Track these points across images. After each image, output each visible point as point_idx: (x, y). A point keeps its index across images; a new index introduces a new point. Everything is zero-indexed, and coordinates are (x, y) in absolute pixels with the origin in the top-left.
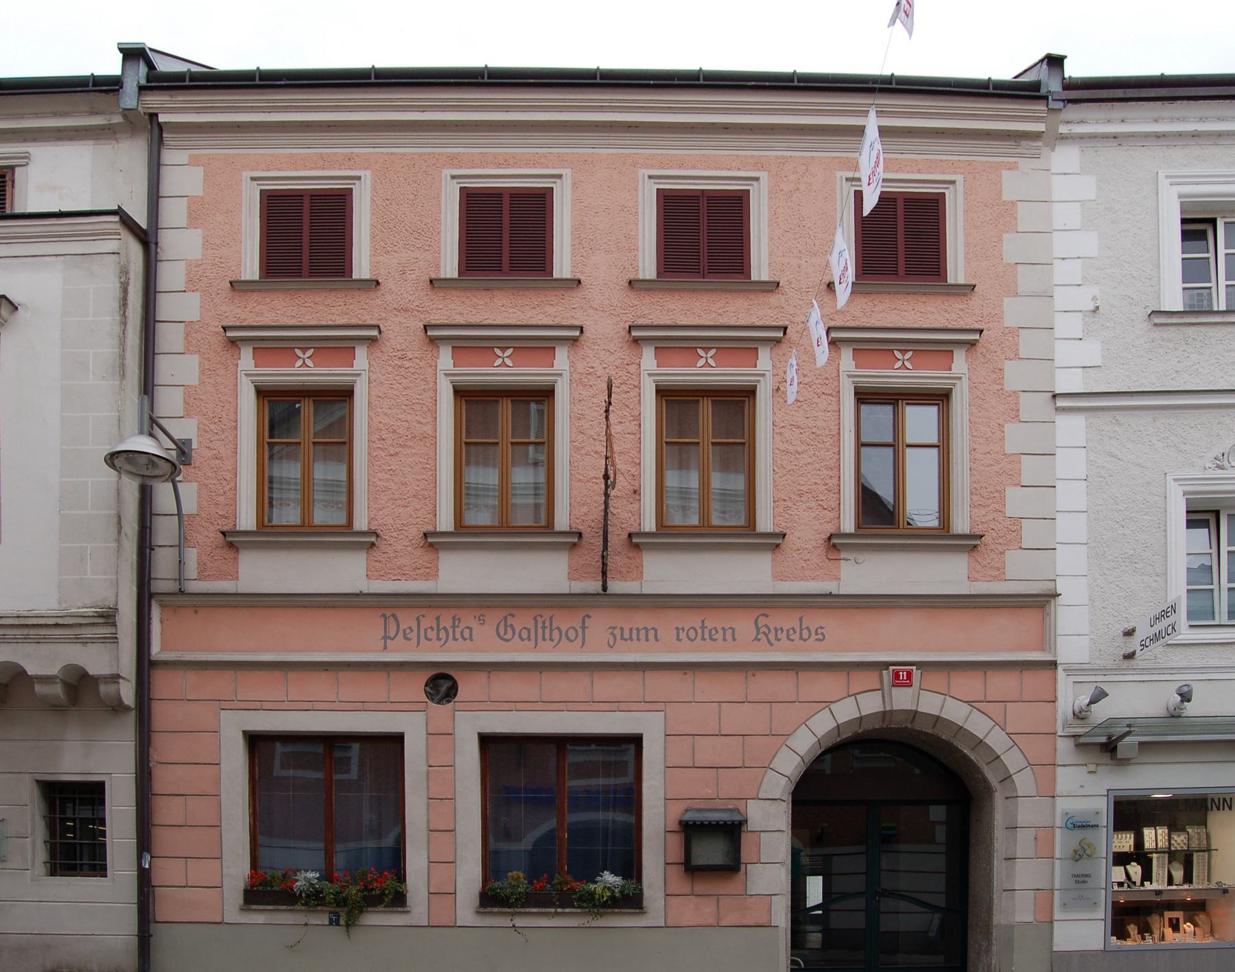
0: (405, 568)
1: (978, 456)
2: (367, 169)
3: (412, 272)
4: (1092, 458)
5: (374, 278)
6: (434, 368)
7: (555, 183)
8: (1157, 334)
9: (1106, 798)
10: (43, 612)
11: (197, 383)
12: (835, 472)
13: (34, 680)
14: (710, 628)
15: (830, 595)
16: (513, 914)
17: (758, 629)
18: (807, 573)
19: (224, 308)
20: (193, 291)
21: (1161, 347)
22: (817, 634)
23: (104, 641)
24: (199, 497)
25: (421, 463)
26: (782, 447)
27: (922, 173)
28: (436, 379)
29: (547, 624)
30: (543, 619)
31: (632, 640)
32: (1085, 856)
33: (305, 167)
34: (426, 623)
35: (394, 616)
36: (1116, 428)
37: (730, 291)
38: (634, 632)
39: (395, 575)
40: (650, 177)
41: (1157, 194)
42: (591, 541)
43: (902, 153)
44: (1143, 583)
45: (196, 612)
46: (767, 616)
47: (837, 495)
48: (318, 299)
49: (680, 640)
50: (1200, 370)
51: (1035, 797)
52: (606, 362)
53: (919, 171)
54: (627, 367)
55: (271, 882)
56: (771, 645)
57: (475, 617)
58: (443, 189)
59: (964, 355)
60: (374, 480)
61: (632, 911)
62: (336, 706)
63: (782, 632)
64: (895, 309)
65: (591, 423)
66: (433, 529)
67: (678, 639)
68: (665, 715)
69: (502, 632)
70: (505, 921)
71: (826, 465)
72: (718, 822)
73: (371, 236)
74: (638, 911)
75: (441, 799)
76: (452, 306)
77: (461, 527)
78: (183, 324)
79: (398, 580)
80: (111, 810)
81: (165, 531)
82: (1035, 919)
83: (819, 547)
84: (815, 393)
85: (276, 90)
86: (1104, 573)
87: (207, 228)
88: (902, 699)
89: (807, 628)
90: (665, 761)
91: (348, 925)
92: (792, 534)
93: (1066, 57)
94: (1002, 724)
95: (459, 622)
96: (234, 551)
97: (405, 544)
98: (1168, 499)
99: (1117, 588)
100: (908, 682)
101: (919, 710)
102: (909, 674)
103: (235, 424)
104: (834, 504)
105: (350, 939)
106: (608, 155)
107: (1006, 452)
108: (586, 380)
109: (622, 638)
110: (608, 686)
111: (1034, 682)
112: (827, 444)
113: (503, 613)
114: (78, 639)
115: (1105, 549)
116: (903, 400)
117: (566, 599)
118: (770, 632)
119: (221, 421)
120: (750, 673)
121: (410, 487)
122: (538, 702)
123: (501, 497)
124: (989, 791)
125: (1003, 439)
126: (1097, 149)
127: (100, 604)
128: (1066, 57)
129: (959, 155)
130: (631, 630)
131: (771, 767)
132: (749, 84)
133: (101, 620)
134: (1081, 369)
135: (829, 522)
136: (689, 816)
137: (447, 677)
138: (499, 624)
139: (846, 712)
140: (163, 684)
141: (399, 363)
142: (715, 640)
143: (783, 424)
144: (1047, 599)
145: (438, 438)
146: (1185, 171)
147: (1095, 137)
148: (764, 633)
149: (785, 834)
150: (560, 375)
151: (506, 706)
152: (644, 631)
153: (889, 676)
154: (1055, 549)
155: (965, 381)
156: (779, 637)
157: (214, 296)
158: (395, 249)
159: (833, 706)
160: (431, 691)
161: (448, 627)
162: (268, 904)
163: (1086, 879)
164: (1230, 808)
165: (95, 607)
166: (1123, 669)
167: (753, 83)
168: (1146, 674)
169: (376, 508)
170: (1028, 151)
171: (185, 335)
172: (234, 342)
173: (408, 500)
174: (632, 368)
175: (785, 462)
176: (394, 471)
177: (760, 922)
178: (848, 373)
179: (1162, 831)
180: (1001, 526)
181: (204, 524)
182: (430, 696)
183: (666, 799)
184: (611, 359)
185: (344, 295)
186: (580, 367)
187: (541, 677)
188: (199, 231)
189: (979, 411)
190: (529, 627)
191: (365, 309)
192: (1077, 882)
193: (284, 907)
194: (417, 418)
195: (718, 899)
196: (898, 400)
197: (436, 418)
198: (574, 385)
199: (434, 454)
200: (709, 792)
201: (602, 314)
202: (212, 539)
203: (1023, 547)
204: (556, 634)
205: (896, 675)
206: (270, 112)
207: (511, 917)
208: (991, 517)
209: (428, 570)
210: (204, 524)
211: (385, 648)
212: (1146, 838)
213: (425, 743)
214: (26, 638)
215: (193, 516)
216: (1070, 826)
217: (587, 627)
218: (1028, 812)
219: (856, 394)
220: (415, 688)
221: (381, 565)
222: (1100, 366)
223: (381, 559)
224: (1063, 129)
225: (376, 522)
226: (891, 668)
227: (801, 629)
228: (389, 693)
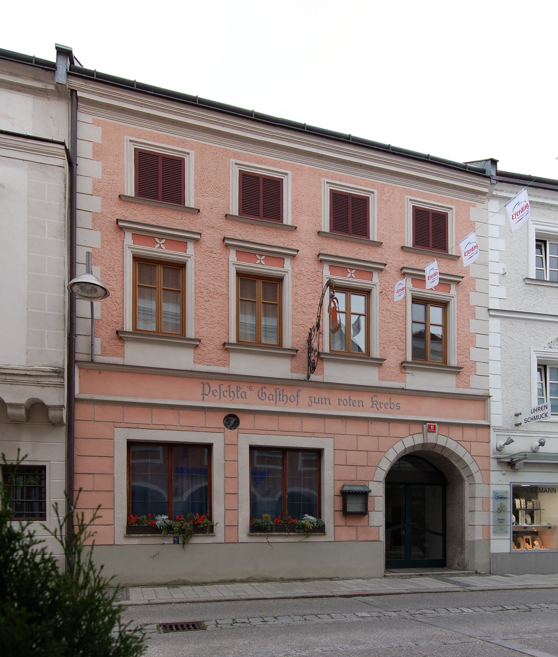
0: (213, 360)
1: (460, 333)
2: (192, 149)
3: (216, 209)
4: (502, 338)
6: (227, 260)
7: (284, 177)
8: (527, 287)
10: (16, 367)
11: (100, 247)
12: (404, 333)
13: (8, 406)
14: (353, 400)
15: (403, 389)
16: (267, 536)
17: (373, 402)
18: (393, 378)
19: (115, 209)
20: (97, 196)
21: (528, 293)
22: (397, 406)
23: (56, 386)
24: (102, 310)
25: (221, 307)
26: (383, 319)
28: (228, 265)
29: (281, 393)
30: (279, 390)
31: (319, 403)
32: (502, 511)
33: (159, 141)
35: (207, 383)
36: (512, 327)
37: (361, 243)
38: (320, 400)
39: (208, 363)
40: (327, 183)
41: (528, 227)
42: (301, 355)
45: (100, 373)
46: (266, 388)
47: (405, 344)
48: (167, 214)
49: (340, 405)
50: (542, 305)
53: (438, 201)
54: (317, 273)
55: (142, 521)
56: (378, 410)
57: (247, 387)
58: (231, 169)
59: (455, 288)
60: (198, 313)
61: (320, 534)
62: (178, 428)
63: (341, 401)
65: (301, 297)
66: (227, 341)
68: (334, 440)
69: (260, 396)
70: (265, 540)
72: (359, 491)
73: (194, 185)
74: (323, 534)
76: (236, 230)
77: (239, 342)
78: (91, 213)
79: (210, 365)
80: (50, 482)
81: (83, 327)
82: (483, 539)
83: (397, 367)
85: (147, 96)
87: (104, 162)
88: (432, 438)
89: (393, 403)
90: (334, 462)
91: (184, 543)
93: (498, 161)
94: (469, 451)
95: (240, 389)
96: (122, 342)
97: (213, 347)
98: (531, 359)
99: (512, 395)
101: (437, 443)
102: (435, 427)
103: (122, 273)
104: (404, 348)
105: (185, 550)
106: (308, 168)
108: (298, 276)
109: (315, 402)
110: (310, 425)
111: (481, 433)
112: (401, 320)
113: (261, 386)
114: (38, 384)
116: (429, 303)
117: (277, 381)
119: (114, 270)
120: (370, 422)
121: (216, 319)
123: (181, 325)
124: (461, 480)
125: (469, 326)
127: (53, 365)
128: (498, 161)
130: (319, 398)
132: (374, 147)
133: (55, 374)
136: (346, 488)
137: (234, 416)
138: (259, 391)
139: (409, 442)
140: (81, 412)
141: (210, 254)
142: (355, 406)
143: (383, 309)
145: (230, 295)
146: (538, 219)
147: (505, 198)
148: (375, 404)
150: (287, 272)
152: (324, 399)
153: (426, 427)
154: (488, 376)
155: (455, 298)
156: (381, 407)
157: (109, 200)
158: (207, 195)
159: (403, 440)
160: (226, 423)
161: (235, 391)
162: (141, 533)
163: (503, 521)
164: (555, 492)
165: (51, 366)
167: (376, 147)
169: (198, 327)
170: (480, 200)
171: (93, 219)
173: (215, 325)
174: (319, 274)
175: (384, 326)
176: (207, 309)
177: (375, 539)
179: (523, 501)
181: (105, 325)
182: (226, 425)
183: (334, 480)
184: (310, 268)
185: (181, 214)
186: (296, 269)
187: (279, 419)
188: (100, 163)
191: (192, 223)
192: (500, 522)
193: (150, 535)
194: (219, 284)
195: (357, 528)
196: (427, 303)
197: (228, 285)
198: (293, 278)
199: (227, 303)
200: (353, 477)
201: (305, 245)
202: (109, 334)
204: (285, 398)
205: (429, 427)
206: (142, 107)
207: (266, 538)
208: (465, 360)
209: (225, 361)
210: (105, 325)
211: (203, 399)
212: (517, 504)
213: (223, 449)
214: (4, 381)
215: (98, 320)
216: (496, 497)
218: (480, 491)
219: (412, 299)
220: (218, 421)
221: (201, 357)
223: (201, 354)
224: (494, 193)
225: (199, 335)
226: (428, 424)
227: (390, 404)
228: (205, 423)
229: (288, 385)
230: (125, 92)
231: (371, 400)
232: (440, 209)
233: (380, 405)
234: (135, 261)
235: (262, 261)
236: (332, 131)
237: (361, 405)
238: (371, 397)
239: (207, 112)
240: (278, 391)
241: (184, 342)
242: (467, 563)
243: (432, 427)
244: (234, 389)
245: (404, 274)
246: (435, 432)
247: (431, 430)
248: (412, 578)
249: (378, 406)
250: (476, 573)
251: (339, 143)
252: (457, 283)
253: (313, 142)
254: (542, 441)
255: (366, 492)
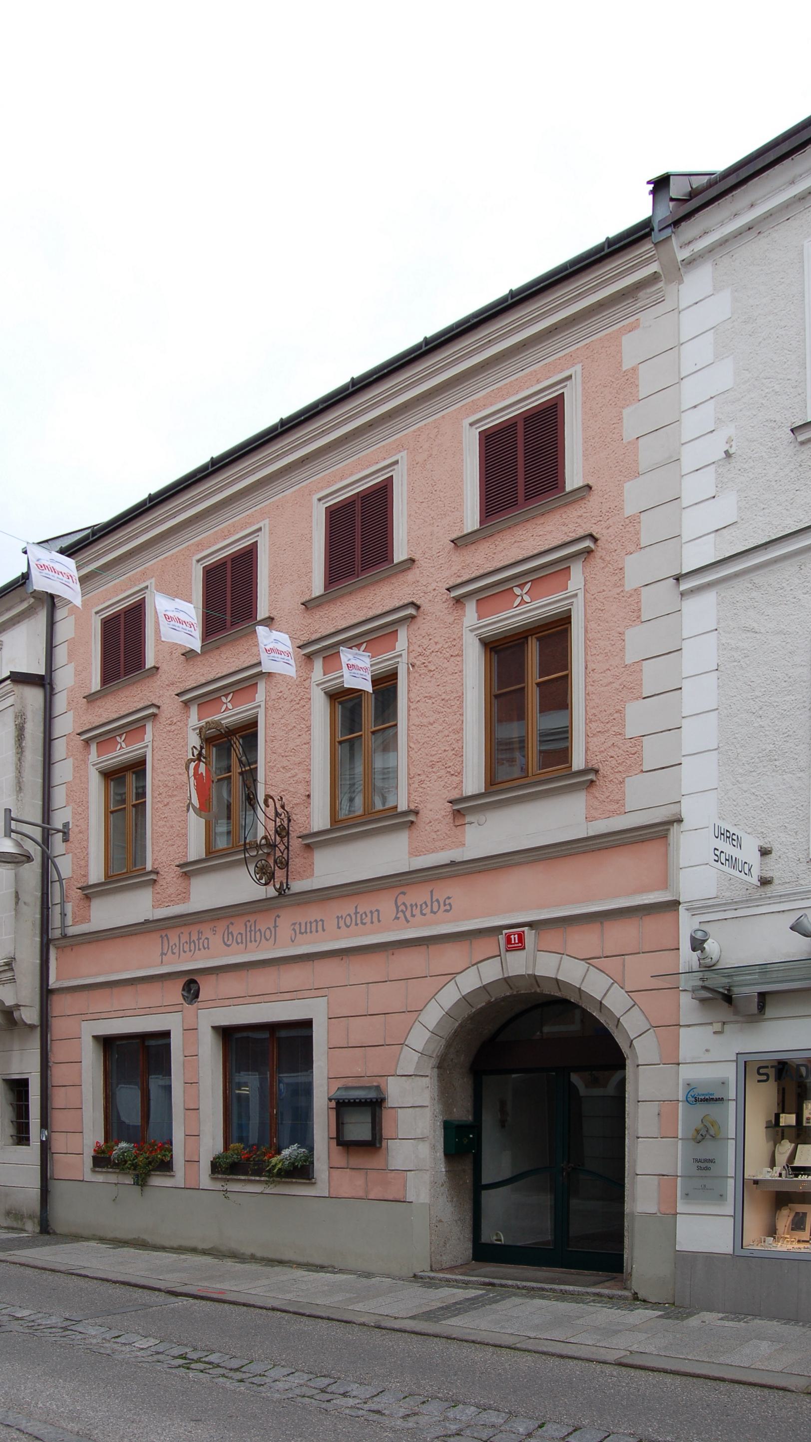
5: (586, 483)
9: (735, 1064)
14: (361, 913)
15: (453, 863)
17: (397, 907)
22: (445, 905)
27: (541, 382)
29: (253, 928)
32: (708, 1136)
34: (235, 930)
35: (166, 935)
43: (522, 370)
44: (784, 784)
46: (404, 893)
51: (659, 1064)
52: (290, 683)
53: (538, 381)
63: (342, 919)
64: (515, 542)
67: (339, 928)
71: (454, 729)
72: (355, 1100)
74: (308, 1181)
75: (192, 1083)
77: (211, 852)
82: (659, 1210)
83: (448, 815)
84: (445, 658)
86: (738, 781)
92: (425, 807)
99: (753, 797)
100: (520, 945)
102: (521, 937)
107: (626, 664)
109: (301, 933)
111: (653, 925)
115: (740, 750)
117: (246, 907)
118: (406, 909)
122: (426, 977)
125: (623, 649)
126: (731, 254)
129: (578, 342)
130: (306, 923)
131: (406, 1043)
132: (371, 379)
134: (713, 535)
135: (456, 788)
139: (469, 982)
140: (59, 1005)
144: (666, 827)
147: (727, 241)
148: (402, 911)
149: (428, 1109)
151: (227, 1002)
156: (414, 913)
163: (709, 1165)
165: (5, 959)
166: (756, 899)
168: (785, 902)
170: (648, 301)
172: (458, 601)
177: (398, 1198)
178: (470, 628)
180: (620, 751)
189: (599, 625)
190: (242, 932)
192: (699, 1168)
200: (358, 1070)
203: (644, 770)
208: (610, 744)
216: (691, 1099)
217: (278, 927)
220: (174, 993)
222: (736, 522)
226: (505, 932)
227: (432, 903)
229: (261, 911)
230: (136, 523)
231: (394, 905)
232: (125, 603)
233: (412, 910)
234: (333, 701)
235: (520, 598)
236: (339, 388)
237: (375, 919)
238: (274, 917)
239: (295, 434)
240: (248, 924)
241: (534, 790)
242: (629, 1271)
243: (514, 938)
244: (195, 937)
245: (458, 601)
246: (524, 948)
247: (516, 944)
248: (472, 1288)
249: (407, 914)
250: (636, 1297)
251: (321, 416)
252: (585, 555)
253: (282, 448)
254: (699, 935)
255: (360, 1101)
